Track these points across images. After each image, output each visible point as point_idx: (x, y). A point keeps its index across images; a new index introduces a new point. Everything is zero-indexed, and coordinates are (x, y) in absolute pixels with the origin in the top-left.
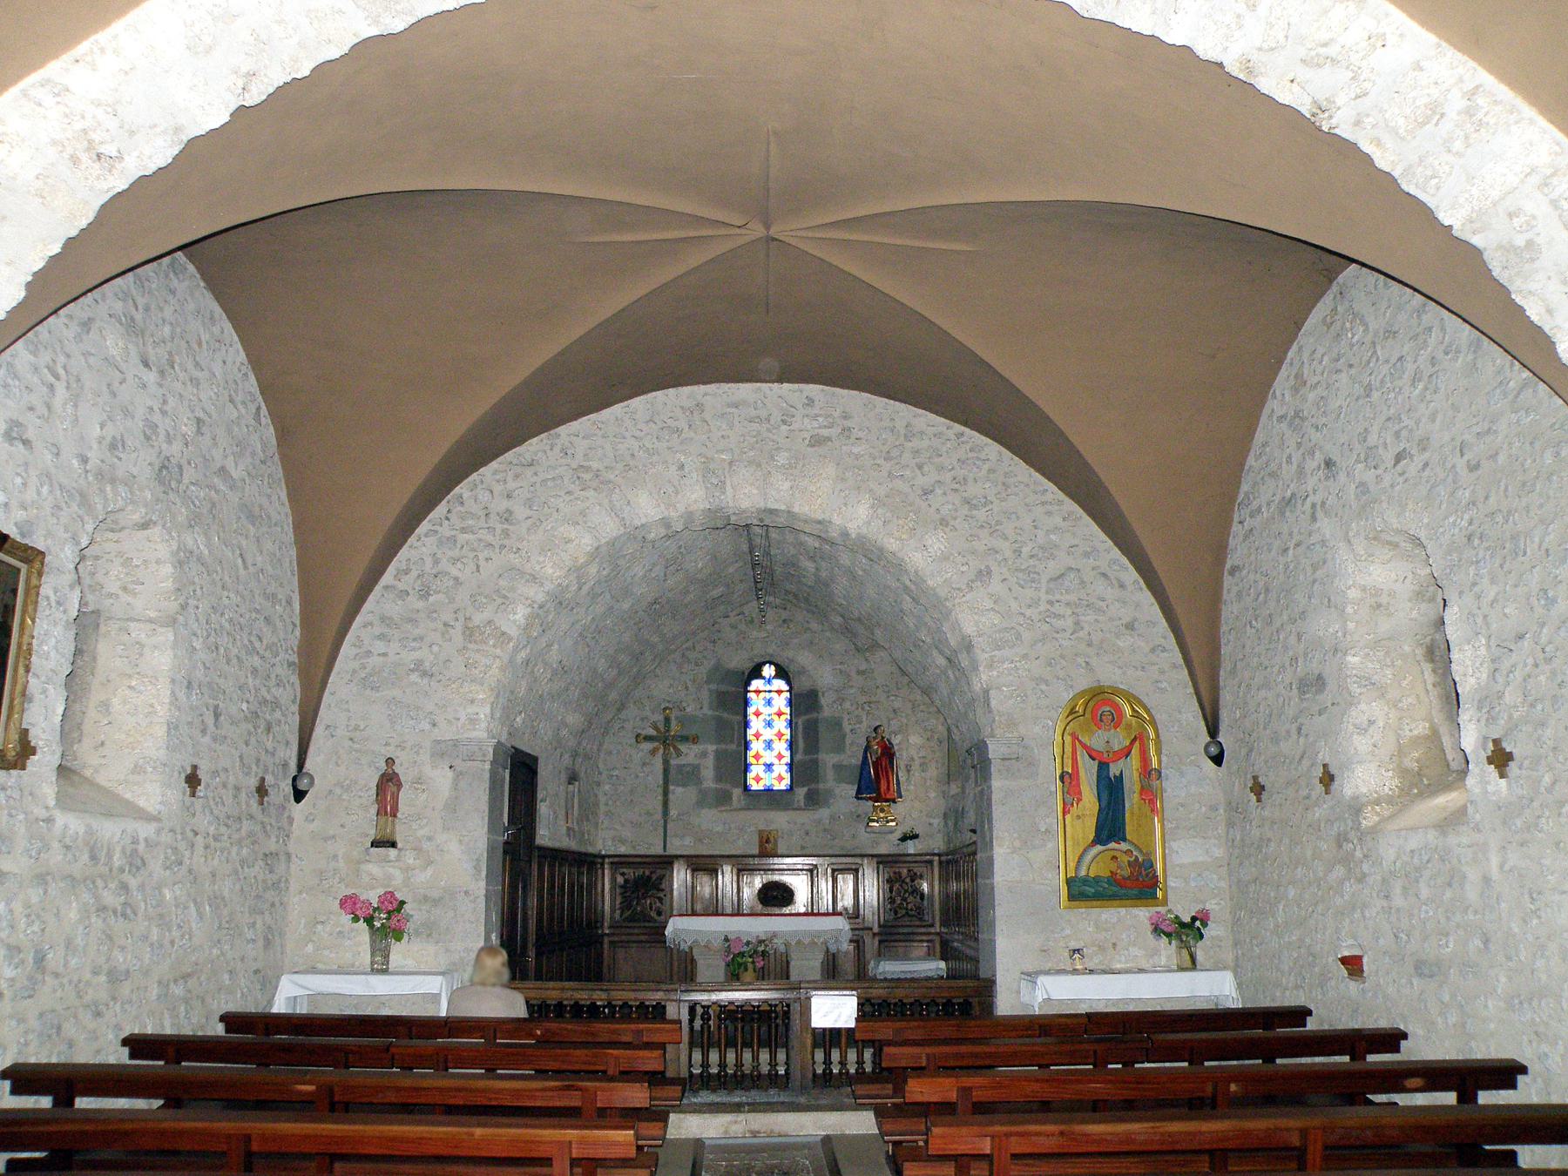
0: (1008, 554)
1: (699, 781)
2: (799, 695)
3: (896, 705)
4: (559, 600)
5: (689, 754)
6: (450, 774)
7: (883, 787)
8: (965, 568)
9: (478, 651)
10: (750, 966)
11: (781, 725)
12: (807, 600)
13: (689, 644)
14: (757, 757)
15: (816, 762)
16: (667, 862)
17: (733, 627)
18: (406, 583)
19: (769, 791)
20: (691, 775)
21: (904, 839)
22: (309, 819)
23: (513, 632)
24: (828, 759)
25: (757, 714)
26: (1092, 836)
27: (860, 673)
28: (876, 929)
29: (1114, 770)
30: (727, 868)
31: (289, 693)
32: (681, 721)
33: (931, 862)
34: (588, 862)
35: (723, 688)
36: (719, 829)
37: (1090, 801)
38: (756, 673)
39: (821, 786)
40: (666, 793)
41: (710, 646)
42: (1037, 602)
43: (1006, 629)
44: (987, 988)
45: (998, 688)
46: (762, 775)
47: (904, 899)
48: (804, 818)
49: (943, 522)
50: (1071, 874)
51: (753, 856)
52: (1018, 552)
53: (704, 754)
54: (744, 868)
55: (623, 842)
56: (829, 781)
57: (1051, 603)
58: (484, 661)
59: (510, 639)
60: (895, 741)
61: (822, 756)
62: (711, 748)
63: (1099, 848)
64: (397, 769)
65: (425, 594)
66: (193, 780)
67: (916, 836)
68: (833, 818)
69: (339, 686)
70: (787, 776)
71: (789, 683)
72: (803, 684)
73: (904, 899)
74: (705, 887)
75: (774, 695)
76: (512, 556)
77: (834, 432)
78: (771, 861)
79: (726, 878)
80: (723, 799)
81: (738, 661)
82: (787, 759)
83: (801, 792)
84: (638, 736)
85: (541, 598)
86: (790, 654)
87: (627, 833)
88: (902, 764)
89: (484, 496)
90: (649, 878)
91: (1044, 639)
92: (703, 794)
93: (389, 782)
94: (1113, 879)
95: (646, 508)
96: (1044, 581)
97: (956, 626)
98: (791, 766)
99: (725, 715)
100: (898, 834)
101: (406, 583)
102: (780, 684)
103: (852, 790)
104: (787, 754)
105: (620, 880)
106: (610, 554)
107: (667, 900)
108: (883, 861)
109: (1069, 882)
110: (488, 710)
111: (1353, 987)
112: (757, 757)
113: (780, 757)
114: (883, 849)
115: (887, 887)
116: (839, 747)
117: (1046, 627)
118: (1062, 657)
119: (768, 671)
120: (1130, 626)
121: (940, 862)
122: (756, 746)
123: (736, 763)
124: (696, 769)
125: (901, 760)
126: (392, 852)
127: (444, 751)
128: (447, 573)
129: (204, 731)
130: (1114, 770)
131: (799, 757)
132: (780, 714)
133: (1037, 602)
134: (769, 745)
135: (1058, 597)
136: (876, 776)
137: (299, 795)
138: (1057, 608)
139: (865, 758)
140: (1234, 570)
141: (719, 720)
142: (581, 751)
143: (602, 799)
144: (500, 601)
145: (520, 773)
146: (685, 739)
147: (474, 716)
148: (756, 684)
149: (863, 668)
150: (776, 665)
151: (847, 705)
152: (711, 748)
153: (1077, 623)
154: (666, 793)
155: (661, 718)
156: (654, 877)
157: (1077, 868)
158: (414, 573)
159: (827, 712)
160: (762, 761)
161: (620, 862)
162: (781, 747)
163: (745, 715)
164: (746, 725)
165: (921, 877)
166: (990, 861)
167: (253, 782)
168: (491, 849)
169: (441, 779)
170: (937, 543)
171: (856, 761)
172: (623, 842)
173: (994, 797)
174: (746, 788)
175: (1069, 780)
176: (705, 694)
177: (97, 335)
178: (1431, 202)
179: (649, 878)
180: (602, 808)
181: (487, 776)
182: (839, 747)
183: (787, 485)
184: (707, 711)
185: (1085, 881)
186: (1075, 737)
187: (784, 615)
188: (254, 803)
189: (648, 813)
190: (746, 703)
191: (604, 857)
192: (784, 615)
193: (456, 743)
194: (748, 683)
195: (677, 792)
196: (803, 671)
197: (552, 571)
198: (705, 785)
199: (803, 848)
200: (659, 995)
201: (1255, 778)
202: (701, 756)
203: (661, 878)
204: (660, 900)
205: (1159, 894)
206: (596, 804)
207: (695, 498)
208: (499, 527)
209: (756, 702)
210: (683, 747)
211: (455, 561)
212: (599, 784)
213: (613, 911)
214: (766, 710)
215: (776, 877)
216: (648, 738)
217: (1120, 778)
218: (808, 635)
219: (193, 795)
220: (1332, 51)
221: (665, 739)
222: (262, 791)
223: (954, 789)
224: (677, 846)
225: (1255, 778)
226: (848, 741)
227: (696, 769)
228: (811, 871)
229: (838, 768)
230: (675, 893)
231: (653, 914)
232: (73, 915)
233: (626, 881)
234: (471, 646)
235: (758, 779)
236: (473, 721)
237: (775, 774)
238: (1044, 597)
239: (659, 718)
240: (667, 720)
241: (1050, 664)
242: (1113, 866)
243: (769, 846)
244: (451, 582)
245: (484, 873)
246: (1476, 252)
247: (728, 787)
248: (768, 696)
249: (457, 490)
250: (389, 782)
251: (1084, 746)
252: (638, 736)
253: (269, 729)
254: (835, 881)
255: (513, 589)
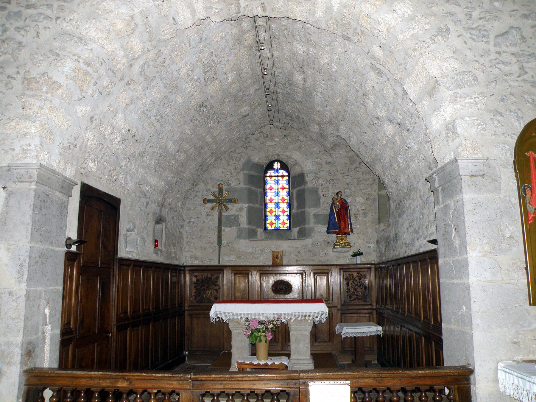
0: (461, 16)
1: (239, 224)
2: (295, 177)
3: (348, 181)
5: (233, 209)
7: (343, 225)
8: (427, 27)
9: (33, 96)
10: (263, 339)
11: (284, 194)
12: (298, 117)
13: (233, 149)
15: (304, 213)
16: (219, 269)
17: (257, 140)
19: (277, 229)
20: (234, 221)
21: (355, 255)
24: (311, 211)
25: (271, 189)
27: (328, 163)
28: (339, 307)
30: (255, 273)
32: (229, 192)
33: (370, 268)
34: (178, 269)
35: (253, 173)
36: (250, 250)
38: (270, 166)
39: (307, 226)
40: (220, 232)
41: (244, 150)
43: (464, 73)
45: (462, 118)
46: (274, 221)
47: (355, 289)
48: (298, 244)
51: (269, 266)
52: (469, 16)
53: (241, 209)
54: (264, 271)
56: (311, 223)
57: (498, 53)
58: (38, 104)
59: (60, 86)
60: (349, 200)
61: (307, 209)
62: (245, 206)
67: (361, 254)
68: (314, 244)
70: (287, 222)
71: (288, 171)
72: (295, 171)
73: (355, 289)
74: (242, 284)
75: (280, 178)
76: (65, 24)
78: (279, 268)
79: (254, 277)
80: (252, 235)
81: (259, 158)
82: (287, 213)
83: (295, 230)
84: (204, 200)
86: (289, 154)
87: (199, 254)
88: (352, 213)
90: (210, 278)
91: (496, 80)
92: (240, 231)
96: (492, 37)
98: (289, 216)
99: (253, 188)
100: (351, 253)
102: (283, 172)
103: (324, 228)
104: (287, 210)
105: (194, 279)
107: (220, 290)
108: (342, 268)
112: (271, 212)
113: (283, 211)
114: (342, 262)
115: (345, 282)
116: (317, 204)
117: (496, 71)
118: (513, 95)
119: (276, 165)
121: (376, 268)
122: (271, 206)
123: (259, 215)
124: (237, 217)
125: (353, 209)
128: (13, 39)
131: (294, 211)
134: (277, 205)
135: (504, 48)
136: (339, 220)
138: (504, 57)
139: (332, 210)
141: (250, 192)
142: (166, 204)
143: (185, 235)
144: (53, 57)
146: (230, 201)
149: (329, 160)
151: (321, 181)
152: (245, 206)
153: (522, 68)
154: (220, 232)
155: (217, 190)
156: (213, 278)
159: (309, 185)
160: (273, 214)
161: (195, 269)
162: (284, 206)
163: (264, 189)
164: (265, 194)
165: (365, 277)
171: (327, 212)
172: (196, 258)
174: (265, 229)
176: (241, 177)
179: (210, 278)
180: (185, 240)
182: (317, 204)
184: (243, 185)
187: (285, 132)
190: (265, 182)
191: (185, 267)
192: (285, 132)
194: (266, 172)
195: (226, 230)
196: (296, 163)
198: (242, 226)
199: (297, 261)
202: (239, 210)
204: (217, 290)
206: (181, 238)
209: (270, 182)
210: (229, 206)
211: (18, 29)
212: (183, 226)
214: (276, 187)
215: (282, 278)
216: (209, 201)
218: (298, 143)
221: (220, 200)
223: (382, 226)
224: (226, 260)
226: (322, 201)
227: (237, 217)
228: (302, 274)
229: (316, 216)
230: (225, 287)
233: (198, 280)
234: (27, 92)
235: (271, 224)
237: (281, 221)
238: (493, 49)
239: (216, 190)
240: (221, 191)
241: (503, 100)
243: (278, 260)
244: (16, 46)
245: (25, 277)
247: (255, 228)
252: (204, 200)
254: (315, 280)
255: (63, 49)
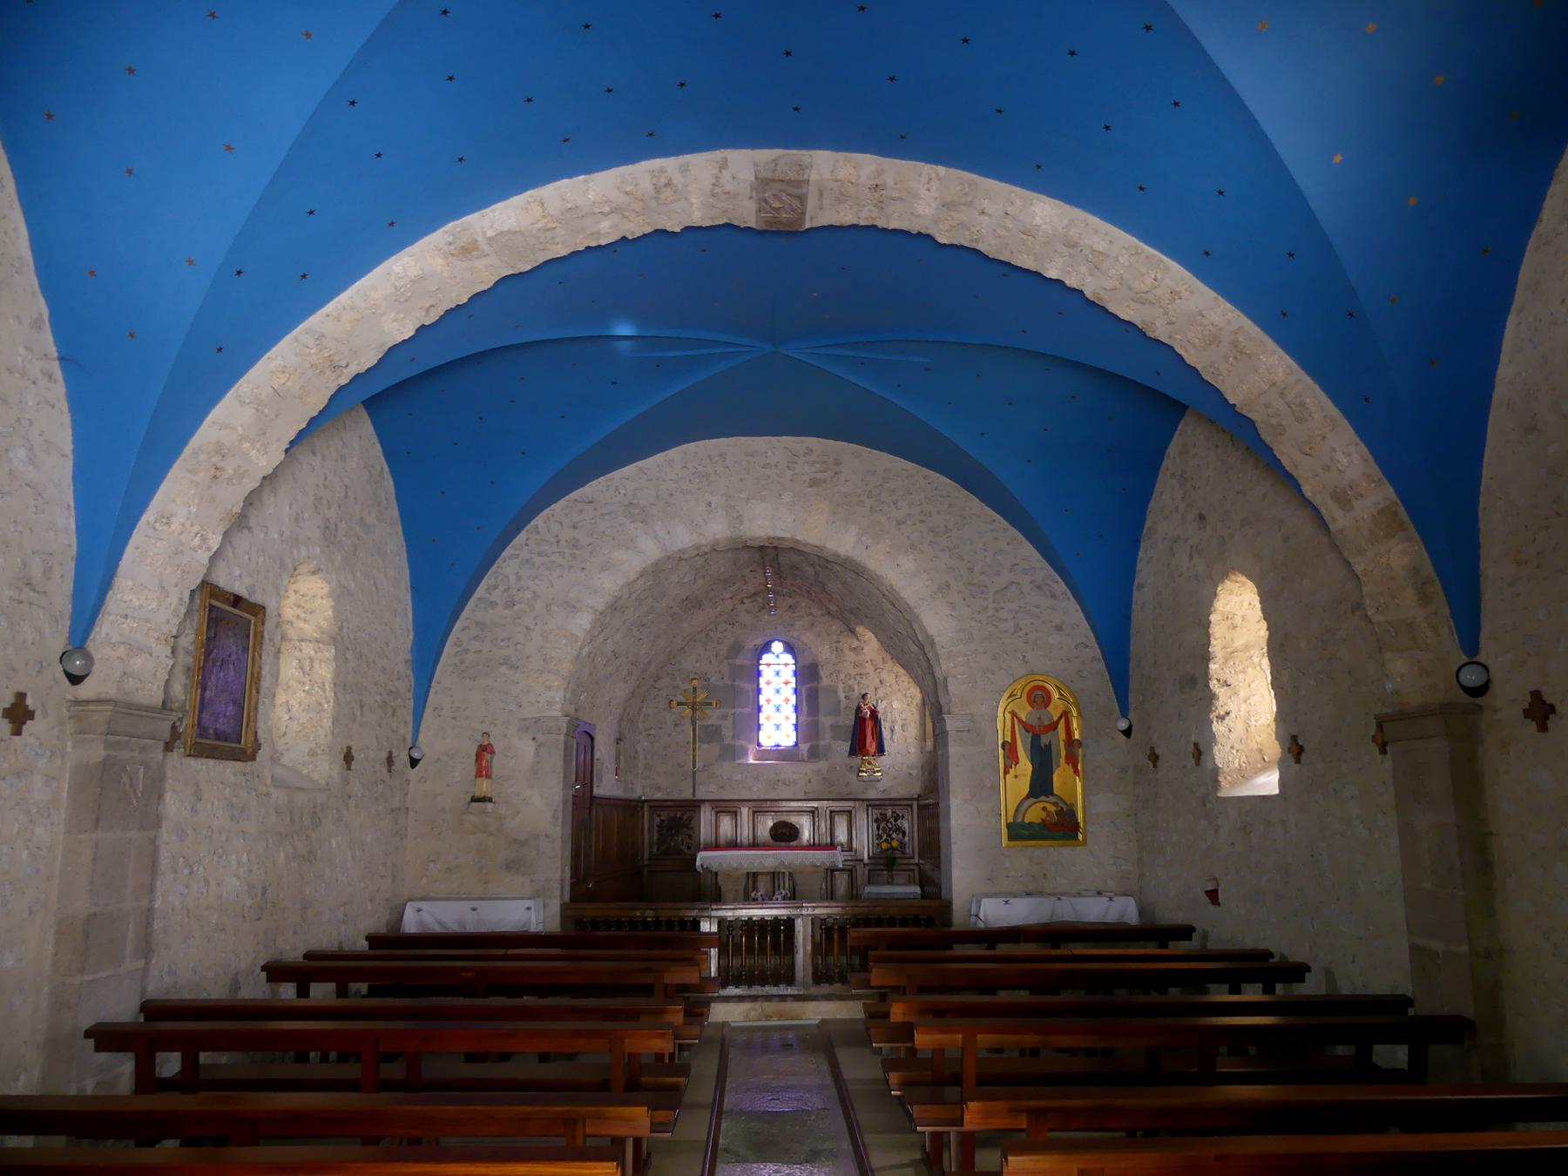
4: (616, 607)
6: (533, 744)
14: (768, 718)
16: (694, 805)
18: (496, 596)
22: (423, 780)
23: (581, 635)
24: (826, 721)
26: (1026, 790)
29: (1044, 740)
31: (405, 683)
37: (1025, 766)
38: (766, 648)
42: (985, 608)
44: (948, 906)
49: (913, 547)
50: (1010, 820)
52: (971, 570)
55: (659, 789)
56: (826, 740)
63: (1032, 800)
64: (493, 741)
65: (510, 604)
66: (348, 758)
69: (443, 674)
71: (795, 657)
74: (726, 824)
77: (829, 474)
85: (601, 607)
89: (555, 527)
93: (484, 750)
94: (1044, 824)
95: (682, 538)
97: (922, 627)
101: (496, 596)
102: (788, 658)
105: (657, 820)
106: (655, 572)
109: (1009, 826)
110: (561, 693)
111: (1212, 908)
120: (1059, 628)
126: (489, 806)
127: (531, 727)
129: (354, 720)
130: (1044, 740)
132: (787, 683)
133: (985, 608)
137: (414, 763)
140: (1141, 586)
145: (582, 739)
147: (549, 697)
148: (766, 658)
150: (785, 643)
157: (1015, 816)
158: (502, 588)
159: (825, 681)
161: (657, 806)
164: (759, 691)
166: (948, 808)
167: (385, 755)
168: (565, 802)
169: (526, 749)
170: (908, 563)
173: (951, 760)
175: (1010, 749)
177: (314, 467)
178: (1222, 389)
181: (562, 746)
183: (791, 519)
185: (1022, 825)
186: (1013, 714)
188: (384, 770)
189: (679, 765)
193: (537, 720)
197: (610, 584)
200: (694, 913)
201: (1152, 749)
203: (690, 819)
205: (1080, 837)
207: (718, 529)
208: (568, 552)
209: (767, 673)
210: (708, 711)
213: (651, 847)
215: (785, 818)
217: (1049, 746)
219: (349, 769)
220: (1150, 296)
222: (390, 761)
225: (1152, 749)
231: (684, 848)
232: (282, 860)
236: (550, 703)
242: (1044, 815)
246: (1252, 422)
248: (777, 668)
249: (533, 522)
250: (484, 750)
251: (1020, 721)
253: (394, 713)
